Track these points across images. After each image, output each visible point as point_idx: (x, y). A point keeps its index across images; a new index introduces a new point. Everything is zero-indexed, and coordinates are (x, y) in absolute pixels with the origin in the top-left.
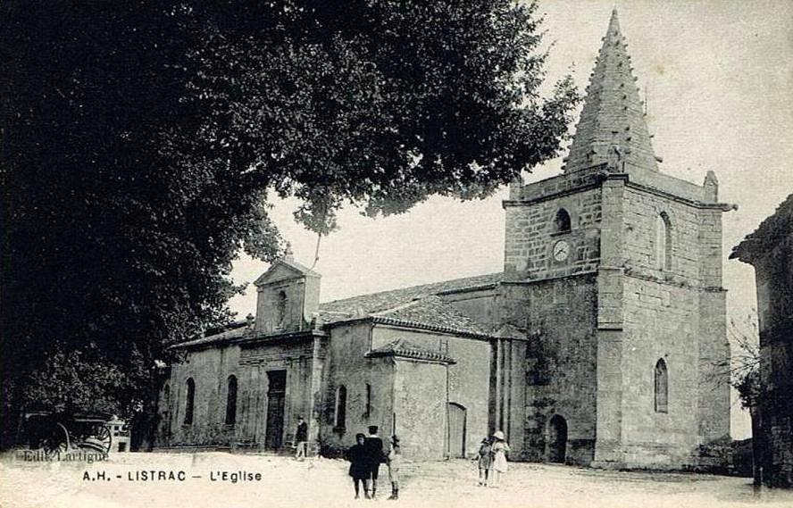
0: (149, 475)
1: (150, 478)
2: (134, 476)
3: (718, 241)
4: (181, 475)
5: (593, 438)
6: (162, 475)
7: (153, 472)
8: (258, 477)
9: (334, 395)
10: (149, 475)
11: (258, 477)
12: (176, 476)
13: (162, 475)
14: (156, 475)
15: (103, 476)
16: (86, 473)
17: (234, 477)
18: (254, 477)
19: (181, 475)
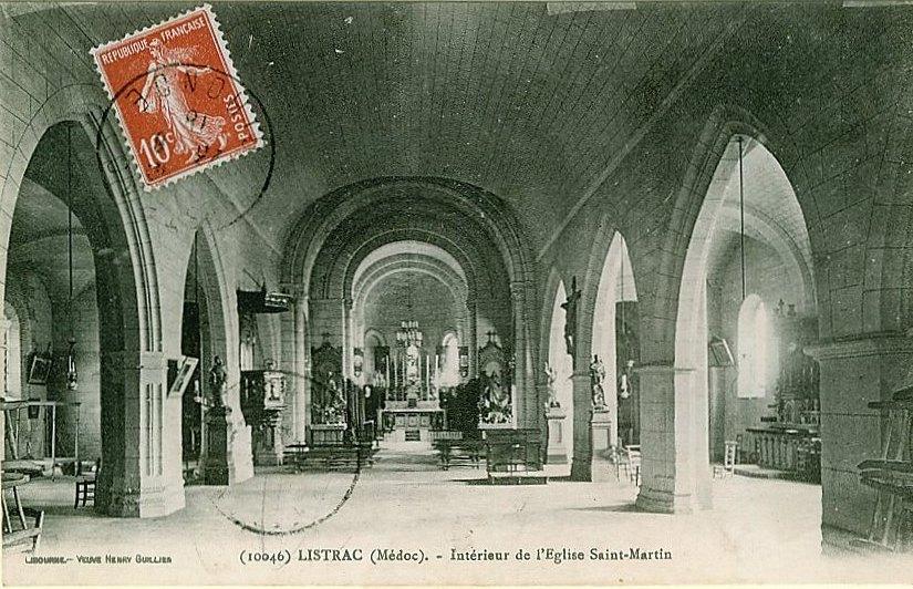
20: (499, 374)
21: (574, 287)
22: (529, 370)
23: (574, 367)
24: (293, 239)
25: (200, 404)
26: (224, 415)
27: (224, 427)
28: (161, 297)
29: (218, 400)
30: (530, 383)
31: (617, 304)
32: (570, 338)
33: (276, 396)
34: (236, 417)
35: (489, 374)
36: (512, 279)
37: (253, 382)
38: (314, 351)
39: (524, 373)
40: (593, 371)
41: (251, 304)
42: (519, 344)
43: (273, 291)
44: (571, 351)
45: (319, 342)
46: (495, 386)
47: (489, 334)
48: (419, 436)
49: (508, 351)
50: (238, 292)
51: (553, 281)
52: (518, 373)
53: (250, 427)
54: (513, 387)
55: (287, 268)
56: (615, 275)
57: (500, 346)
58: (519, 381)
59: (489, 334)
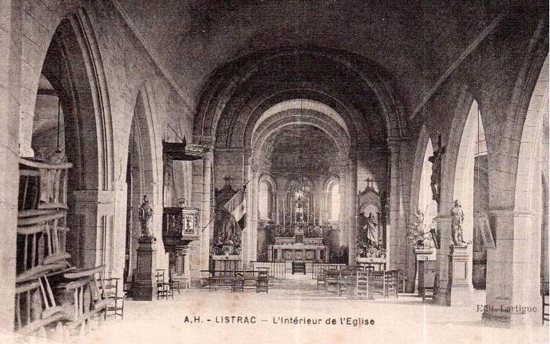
0: (230, 319)
1: (224, 318)
2: (219, 320)
3: (111, 258)
4: (253, 319)
5: (476, 266)
6: (239, 319)
7: (233, 317)
8: (372, 321)
9: (460, 69)
10: (230, 319)
11: (372, 321)
12: (249, 320)
13: (239, 319)
14: (236, 319)
15: (199, 319)
16: (187, 318)
17: (355, 322)
18: (369, 322)
19: (253, 319)
20: (375, 215)
21: (439, 143)
22: (402, 212)
23: (438, 211)
24: (205, 99)
25: (73, 266)
26: (151, 243)
27: (150, 252)
28: (115, 149)
29: (144, 228)
30: (402, 223)
31: (475, 158)
32: (436, 186)
33: (191, 228)
34: (158, 246)
35: (367, 215)
36: (389, 135)
37: (173, 214)
38: (217, 192)
39: (398, 215)
40: (453, 214)
41: (174, 152)
42: (393, 191)
43: (190, 148)
44: (437, 197)
45: (221, 185)
46: (372, 225)
47: (368, 180)
48: (304, 268)
49: (384, 196)
50: (164, 143)
51: (279, 211)
52: (392, 214)
53: (168, 254)
54: (388, 227)
55: (197, 121)
56: (472, 131)
57: (377, 191)
58: (393, 221)
59: (368, 180)
